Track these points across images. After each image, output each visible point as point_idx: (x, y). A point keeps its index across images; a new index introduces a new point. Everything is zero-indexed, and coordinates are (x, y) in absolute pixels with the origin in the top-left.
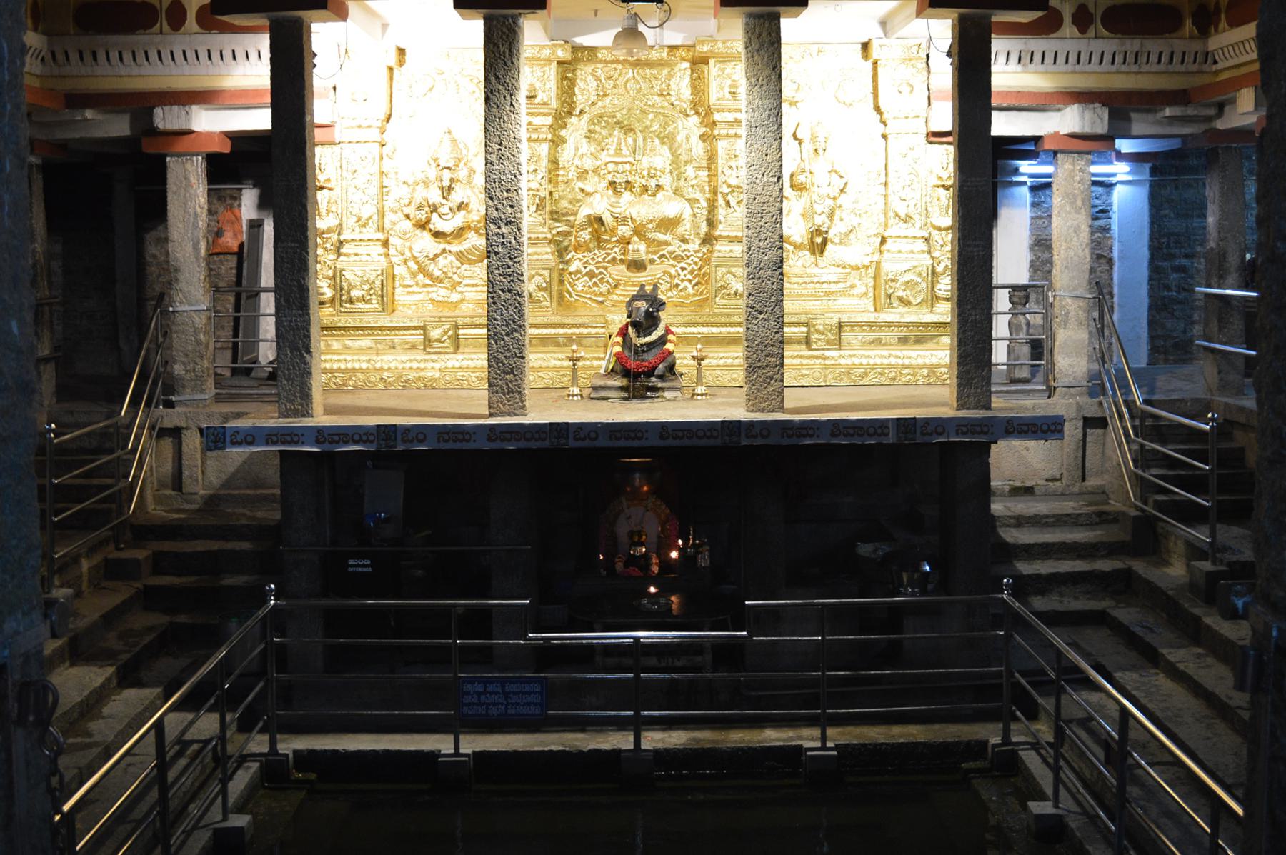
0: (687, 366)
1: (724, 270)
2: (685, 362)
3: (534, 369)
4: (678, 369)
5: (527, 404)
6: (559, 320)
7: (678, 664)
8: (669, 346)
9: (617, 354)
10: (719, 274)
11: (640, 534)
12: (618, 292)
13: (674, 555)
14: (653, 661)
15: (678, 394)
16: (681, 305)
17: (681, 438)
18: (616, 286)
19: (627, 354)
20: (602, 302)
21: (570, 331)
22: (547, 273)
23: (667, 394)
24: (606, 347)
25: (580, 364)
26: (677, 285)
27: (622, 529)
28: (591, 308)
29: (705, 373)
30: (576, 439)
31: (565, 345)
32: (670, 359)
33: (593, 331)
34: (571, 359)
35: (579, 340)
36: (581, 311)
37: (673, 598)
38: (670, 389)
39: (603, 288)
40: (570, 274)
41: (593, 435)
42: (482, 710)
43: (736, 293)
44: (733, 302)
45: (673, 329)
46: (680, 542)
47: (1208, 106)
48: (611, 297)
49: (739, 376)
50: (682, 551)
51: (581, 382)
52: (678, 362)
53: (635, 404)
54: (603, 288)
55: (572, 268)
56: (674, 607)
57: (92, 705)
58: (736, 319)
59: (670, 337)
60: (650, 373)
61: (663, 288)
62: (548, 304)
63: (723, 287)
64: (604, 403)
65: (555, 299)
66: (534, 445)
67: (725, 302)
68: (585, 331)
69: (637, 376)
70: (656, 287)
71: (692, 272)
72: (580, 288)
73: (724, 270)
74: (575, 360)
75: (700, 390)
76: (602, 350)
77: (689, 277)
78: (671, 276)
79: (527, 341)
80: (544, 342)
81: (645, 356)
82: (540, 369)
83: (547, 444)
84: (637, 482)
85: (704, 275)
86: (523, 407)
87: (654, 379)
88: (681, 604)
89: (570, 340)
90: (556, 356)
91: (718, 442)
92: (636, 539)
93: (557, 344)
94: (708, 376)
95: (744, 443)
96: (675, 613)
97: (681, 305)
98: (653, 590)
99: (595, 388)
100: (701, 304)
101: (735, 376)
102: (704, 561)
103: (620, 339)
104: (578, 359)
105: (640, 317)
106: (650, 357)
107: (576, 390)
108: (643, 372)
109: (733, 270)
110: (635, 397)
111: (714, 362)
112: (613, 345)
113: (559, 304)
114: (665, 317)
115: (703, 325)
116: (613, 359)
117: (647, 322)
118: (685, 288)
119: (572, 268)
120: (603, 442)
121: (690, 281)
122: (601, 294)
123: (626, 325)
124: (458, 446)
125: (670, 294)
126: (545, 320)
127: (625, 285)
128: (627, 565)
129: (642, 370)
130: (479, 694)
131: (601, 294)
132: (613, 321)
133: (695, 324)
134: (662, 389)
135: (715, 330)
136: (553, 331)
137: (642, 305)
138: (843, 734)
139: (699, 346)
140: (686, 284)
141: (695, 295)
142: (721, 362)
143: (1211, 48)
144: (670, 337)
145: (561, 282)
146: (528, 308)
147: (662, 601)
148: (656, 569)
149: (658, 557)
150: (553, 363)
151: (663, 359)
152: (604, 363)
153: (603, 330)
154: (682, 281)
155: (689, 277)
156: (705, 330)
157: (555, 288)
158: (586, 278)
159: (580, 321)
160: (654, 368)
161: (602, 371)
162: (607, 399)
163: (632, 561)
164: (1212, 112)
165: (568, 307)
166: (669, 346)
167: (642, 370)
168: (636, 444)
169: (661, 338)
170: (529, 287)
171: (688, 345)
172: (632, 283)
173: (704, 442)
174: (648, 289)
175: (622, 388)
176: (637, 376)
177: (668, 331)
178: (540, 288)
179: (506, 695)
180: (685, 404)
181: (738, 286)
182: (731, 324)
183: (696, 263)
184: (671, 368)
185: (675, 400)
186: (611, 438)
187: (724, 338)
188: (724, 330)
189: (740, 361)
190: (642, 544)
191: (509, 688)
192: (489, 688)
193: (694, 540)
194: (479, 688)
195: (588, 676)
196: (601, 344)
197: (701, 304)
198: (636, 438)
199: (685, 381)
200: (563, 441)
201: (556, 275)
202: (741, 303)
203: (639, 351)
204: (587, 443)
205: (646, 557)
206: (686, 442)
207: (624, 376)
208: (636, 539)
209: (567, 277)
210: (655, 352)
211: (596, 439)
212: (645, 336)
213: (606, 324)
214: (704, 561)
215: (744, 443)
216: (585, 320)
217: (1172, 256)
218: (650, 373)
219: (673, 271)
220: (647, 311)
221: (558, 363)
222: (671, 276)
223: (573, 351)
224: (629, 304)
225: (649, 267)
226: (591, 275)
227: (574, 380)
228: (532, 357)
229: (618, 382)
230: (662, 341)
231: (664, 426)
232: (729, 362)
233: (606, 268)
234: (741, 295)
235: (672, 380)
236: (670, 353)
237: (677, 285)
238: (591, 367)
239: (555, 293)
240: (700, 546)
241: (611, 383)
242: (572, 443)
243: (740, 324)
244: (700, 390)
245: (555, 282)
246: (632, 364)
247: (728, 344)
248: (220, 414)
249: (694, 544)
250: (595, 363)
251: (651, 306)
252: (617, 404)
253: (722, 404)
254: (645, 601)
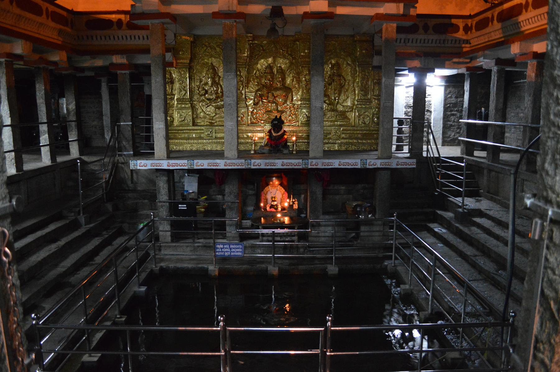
7: (287, 239)
8: (286, 137)
14: (278, 239)
27: (269, 197)
42: (222, 254)
47: (467, 58)
124: (214, 168)
128: (270, 208)
130: (222, 248)
143: (520, 20)
164: (468, 60)
173: (296, 167)
179: (231, 249)
191: (232, 246)
192: (225, 246)
194: (222, 246)
195: (358, 328)
198: (273, 165)
204: (257, 167)
205: (277, 205)
208: (273, 199)
214: (296, 206)
217: (451, 111)
248: (545, 262)
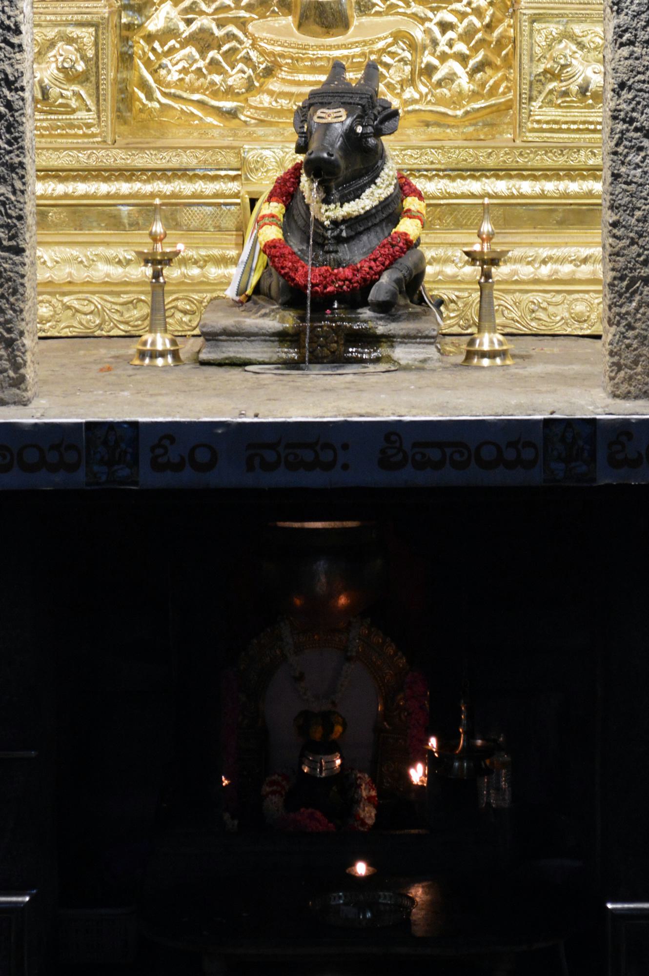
0: (453, 280)
1: (554, 29)
2: (450, 270)
3: (51, 287)
4: (431, 288)
5: (29, 372)
6: (118, 158)
8: (408, 227)
9: (270, 248)
10: (540, 39)
11: (327, 719)
12: (274, 85)
13: (417, 774)
15: (431, 352)
16: (440, 121)
17: (438, 465)
18: (269, 72)
19: (296, 246)
20: (232, 114)
21: (148, 188)
22: (86, 35)
23: (402, 353)
24: (241, 230)
25: (171, 273)
26: (430, 70)
28: (204, 130)
29: (501, 299)
30: (157, 466)
31: (134, 225)
32: (408, 260)
33: (210, 188)
34: (148, 259)
35: (172, 210)
36: (178, 137)
37: (418, 892)
38: (409, 338)
39: (236, 78)
40: (149, 38)
41: (202, 456)
43: (584, 90)
44: (577, 114)
45: (419, 184)
46: (433, 742)
48: (254, 100)
49: (591, 307)
50: (433, 764)
51: (177, 321)
52: (429, 270)
53: (317, 378)
54: (236, 78)
55: (155, 23)
56: (417, 914)
57: (356, 67)
58: (584, 159)
59: (411, 203)
60: (356, 296)
61: (393, 76)
62: (89, 117)
63: (551, 75)
64: (235, 374)
65: (108, 105)
66: (47, 481)
67: (553, 113)
68: (186, 188)
69: (322, 303)
70: (372, 71)
71: (467, 36)
72: (174, 76)
73: (554, 29)
74: (159, 262)
75: (487, 341)
76: (232, 238)
77: (461, 47)
78: (413, 46)
79: (29, 209)
80: (80, 215)
81: (345, 252)
82: (69, 287)
83: (79, 479)
84: (321, 583)
85: (500, 44)
86: (19, 381)
87: (366, 313)
88: (435, 907)
89: (148, 210)
90: (111, 252)
91: (536, 477)
92: (317, 733)
93: (115, 223)
94: (509, 309)
95: (605, 478)
96: (419, 931)
97: (440, 121)
98: (361, 868)
99: (211, 337)
100: (492, 118)
101: (580, 308)
102: (496, 792)
103: (277, 208)
104: (167, 260)
105: (330, 147)
106: (357, 255)
107: (161, 342)
108: (339, 296)
109: (577, 29)
110: (316, 360)
111: (525, 271)
112: (261, 222)
113: (120, 118)
114: (399, 151)
115: (497, 173)
116: (261, 260)
117: (346, 163)
118: (451, 78)
119: (155, 23)
120: (228, 475)
121: (463, 59)
122: (230, 92)
123: (295, 173)
125: (410, 93)
126: (83, 159)
127: (293, 69)
129: (336, 286)
131: (230, 92)
132: (260, 163)
133: (476, 172)
134: (389, 339)
135: (527, 187)
136: (104, 188)
137: (338, 119)
138: (238, 352)
139: (487, 227)
140: (454, 65)
141: (475, 95)
142: (545, 271)
144: (411, 203)
145: (126, 59)
146: (33, 123)
147: (385, 898)
148: (368, 814)
149: (376, 781)
150: (103, 270)
151: (391, 261)
152: (235, 272)
153: (234, 186)
154: (443, 57)
155: (461, 47)
156: (501, 186)
157: (109, 74)
158: (191, 50)
159: (175, 163)
160: (368, 283)
161: (231, 293)
162: (241, 364)
163: (306, 792)
165: (144, 126)
166: (408, 227)
167: (336, 286)
168: (315, 479)
169: (385, 204)
170: (40, 71)
171: (459, 225)
172: (307, 59)
173: (499, 477)
174: (353, 76)
175: (282, 337)
176: (322, 303)
177: (404, 188)
178: (69, 75)
180: (447, 378)
181: (592, 73)
182: (571, 173)
183: (478, 12)
184: (412, 285)
185: (421, 367)
186: (250, 468)
187: (552, 209)
188: (550, 186)
189: (598, 270)
190: (332, 748)
193: (471, 736)
196: (230, 223)
197: (492, 118)
199: (448, 321)
200: (123, 472)
201: (110, 39)
202: (599, 115)
203: (326, 239)
204: (187, 478)
205: (343, 781)
206: (449, 476)
207: (288, 305)
208: (317, 733)
209: (140, 46)
210: (370, 241)
211: (210, 466)
212: (344, 199)
213: (242, 170)
214: (496, 792)
215: (603, 480)
216: (187, 160)
218: (356, 296)
219: (418, 33)
220: (350, 133)
221: (117, 272)
222: (413, 46)
223: (155, 238)
224: (303, 114)
225: (356, 21)
226: (203, 41)
227: (157, 316)
228: (44, 254)
229: (275, 320)
230: (389, 212)
231: (391, 435)
232: (566, 269)
233: (242, 24)
234: (597, 97)
235: (415, 316)
236: (410, 245)
237: (430, 70)
238: (203, 284)
239: (108, 90)
240: (486, 752)
241: (252, 321)
242: (149, 479)
243: (593, 172)
244: (487, 341)
245: (110, 59)
246: (310, 274)
247: (563, 223)
249: (469, 746)
250: (214, 272)
251: (360, 119)
252: (269, 376)
253: (545, 378)
254: (339, 898)
